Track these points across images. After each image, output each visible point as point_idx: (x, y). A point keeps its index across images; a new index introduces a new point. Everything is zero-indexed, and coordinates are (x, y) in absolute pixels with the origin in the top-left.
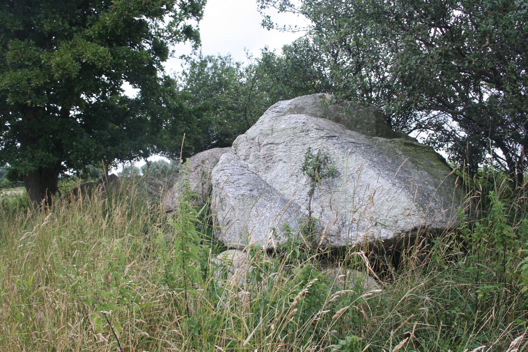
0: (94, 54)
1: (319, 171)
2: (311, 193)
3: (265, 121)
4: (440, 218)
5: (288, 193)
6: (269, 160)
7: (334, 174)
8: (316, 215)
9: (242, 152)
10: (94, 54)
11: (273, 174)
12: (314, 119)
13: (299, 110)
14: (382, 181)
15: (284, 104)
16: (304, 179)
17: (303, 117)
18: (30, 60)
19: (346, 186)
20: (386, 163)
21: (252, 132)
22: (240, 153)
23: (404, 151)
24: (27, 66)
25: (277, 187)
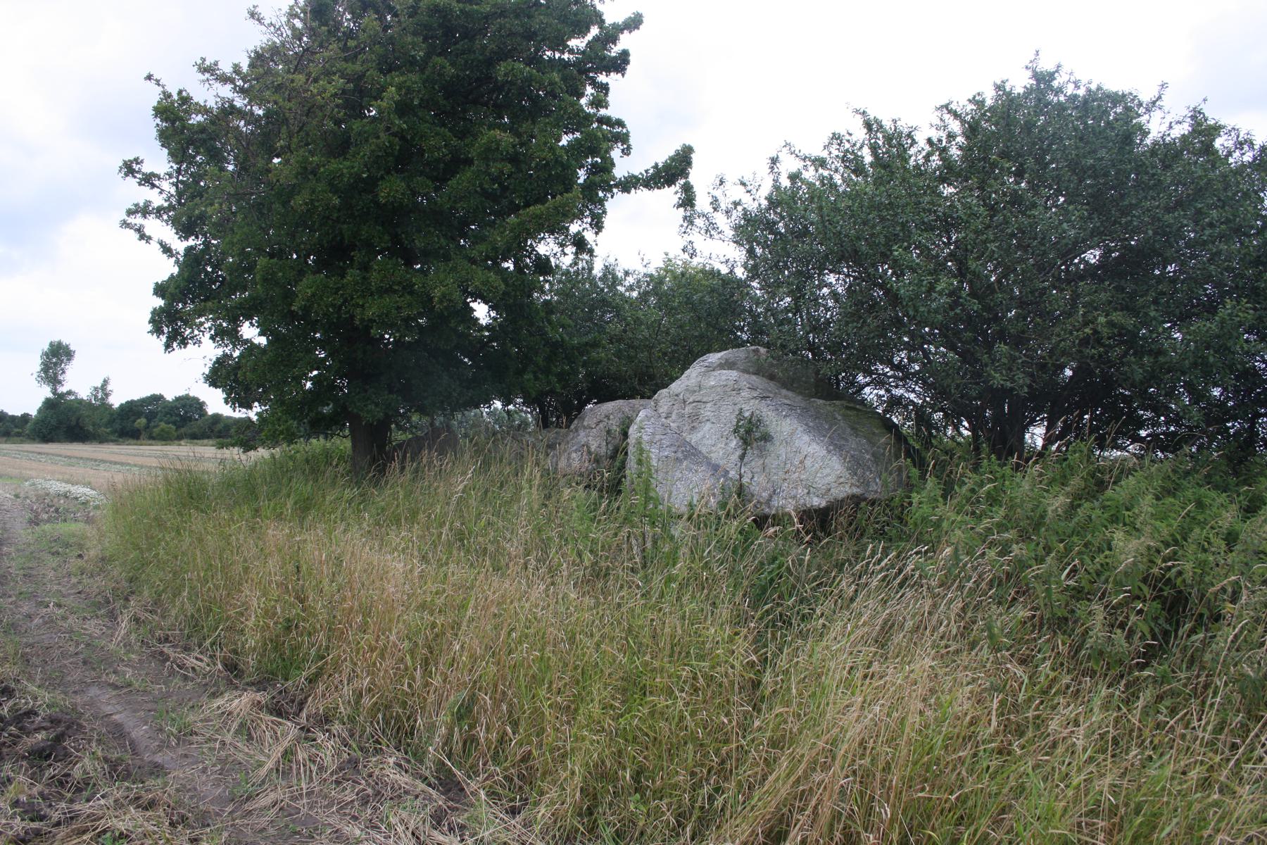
0: (483, 283)
1: (751, 435)
2: (742, 457)
3: (693, 375)
4: (876, 489)
5: (717, 456)
6: (695, 420)
7: (766, 438)
8: (745, 480)
9: (663, 409)
10: (483, 283)
11: (700, 435)
12: (747, 376)
13: (728, 365)
14: (814, 446)
15: (714, 358)
16: (734, 443)
17: (734, 374)
18: (399, 283)
19: (779, 451)
20: (819, 425)
21: (676, 387)
22: (661, 410)
23: (844, 415)
24: (395, 292)
25: (704, 450)
